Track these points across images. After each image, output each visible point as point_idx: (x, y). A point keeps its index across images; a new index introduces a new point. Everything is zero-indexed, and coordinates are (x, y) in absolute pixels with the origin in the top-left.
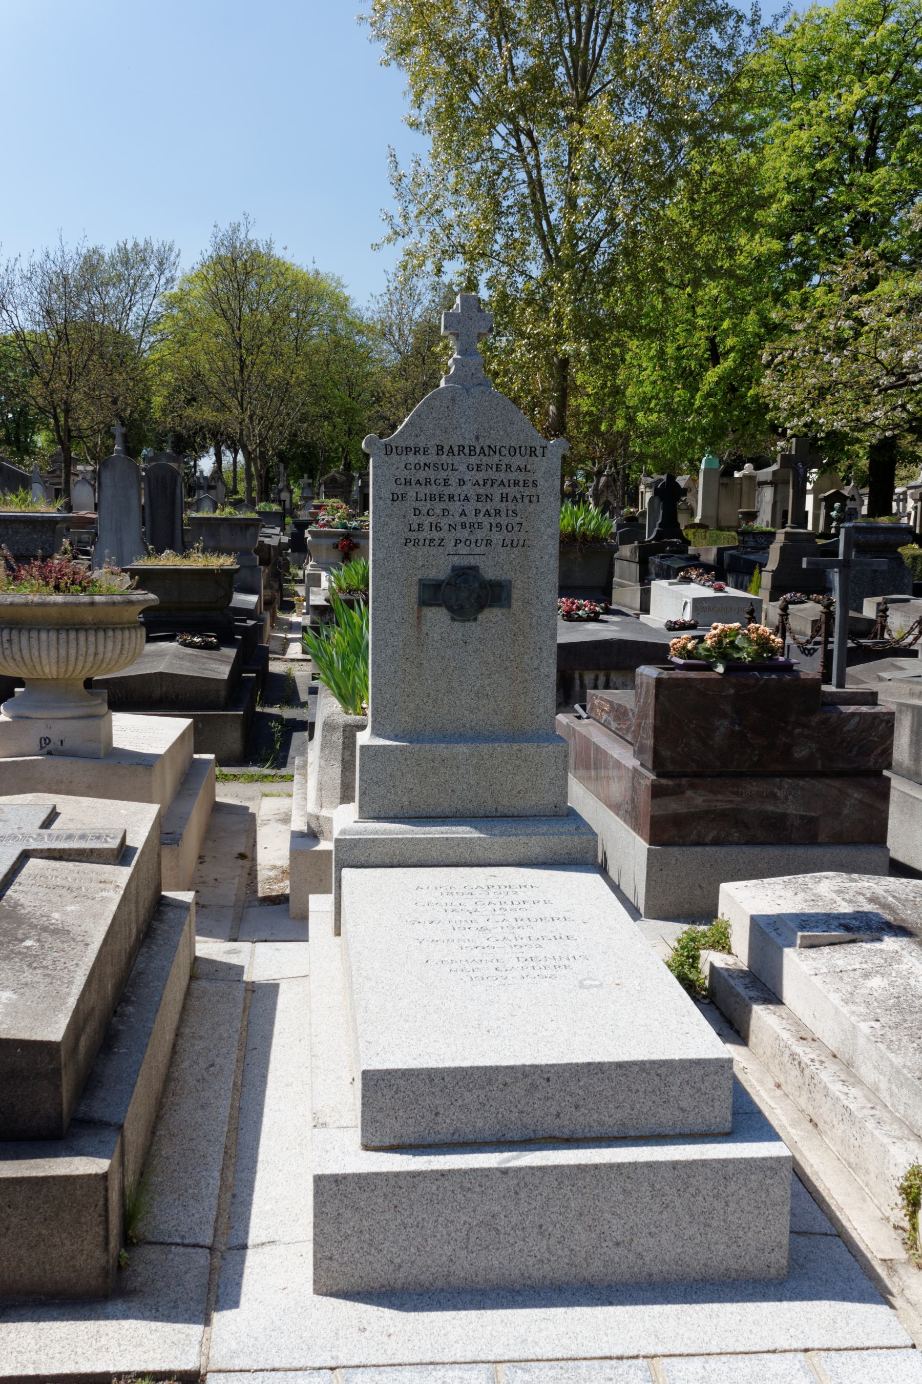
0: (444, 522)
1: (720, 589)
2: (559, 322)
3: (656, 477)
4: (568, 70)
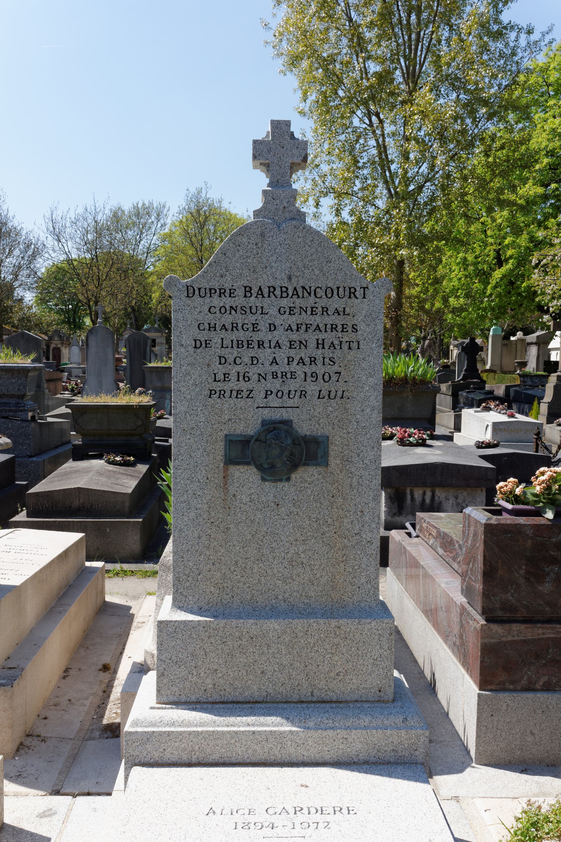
0: (253, 372)
1: (512, 416)
2: (397, 236)
3: (461, 340)
4: (403, 72)
